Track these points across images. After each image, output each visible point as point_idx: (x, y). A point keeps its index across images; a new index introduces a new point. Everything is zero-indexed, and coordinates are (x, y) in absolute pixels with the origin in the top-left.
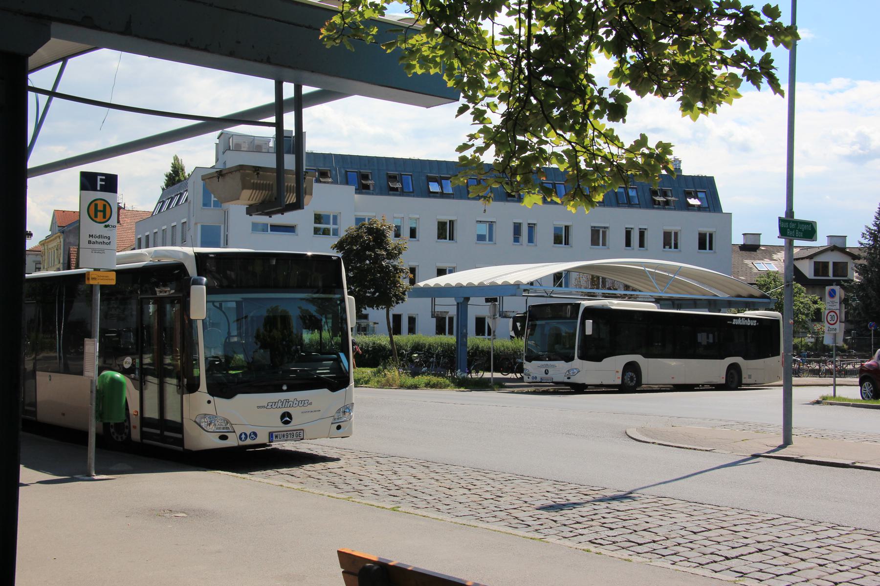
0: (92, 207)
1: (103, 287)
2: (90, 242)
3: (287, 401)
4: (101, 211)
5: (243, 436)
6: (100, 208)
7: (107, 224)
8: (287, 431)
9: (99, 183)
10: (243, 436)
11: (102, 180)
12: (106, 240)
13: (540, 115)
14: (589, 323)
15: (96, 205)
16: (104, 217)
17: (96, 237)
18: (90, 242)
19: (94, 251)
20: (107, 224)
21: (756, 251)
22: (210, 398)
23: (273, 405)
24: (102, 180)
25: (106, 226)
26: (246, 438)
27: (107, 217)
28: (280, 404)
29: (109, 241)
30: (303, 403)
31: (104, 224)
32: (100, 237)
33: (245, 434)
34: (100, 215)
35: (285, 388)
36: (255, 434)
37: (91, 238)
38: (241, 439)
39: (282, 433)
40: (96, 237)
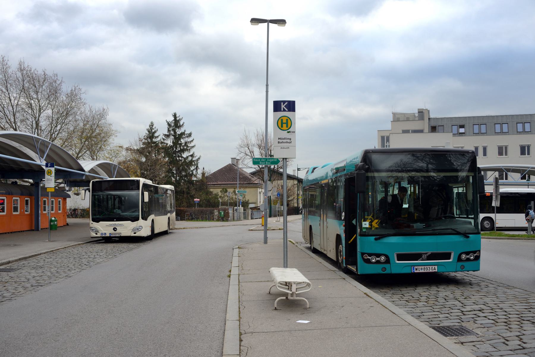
0: (280, 121)
1: (51, 192)
2: (279, 142)
3: (115, 224)
4: (285, 123)
5: (102, 234)
6: (284, 121)
7: (289, 131)
8: (425, 266)
9: (49, 165)
10: (102, 234)
11: (50, 164)
12: (280, 141)
13: (136, 147)
14: (146, 194)
15: (282, 120)
16: (50, 174)
17: (282, 139)
18: (279, 142)
19: (48, 183)
20: (289, 131)
21: (355, 165)
22: (92, 222)
23: (111, 225)
24: (50, 164)
25: (288, 132)
26: (103, 234)
27: (289, 126)
28: (113, 225)
29: (290, 141)
30: (121, 225)
31: (287, 131)
32: (284, 139)
33: (103, 234)
34: (285, 125)
35: (115, 220)
36: (105, 234)
37: (279, 140)
38: (101, 235)
39: (421, 267)
40: (282, 139)
